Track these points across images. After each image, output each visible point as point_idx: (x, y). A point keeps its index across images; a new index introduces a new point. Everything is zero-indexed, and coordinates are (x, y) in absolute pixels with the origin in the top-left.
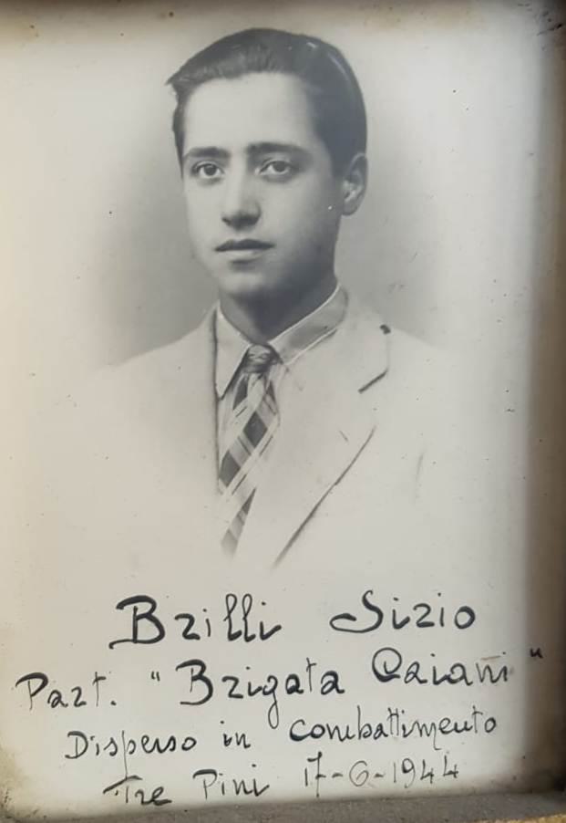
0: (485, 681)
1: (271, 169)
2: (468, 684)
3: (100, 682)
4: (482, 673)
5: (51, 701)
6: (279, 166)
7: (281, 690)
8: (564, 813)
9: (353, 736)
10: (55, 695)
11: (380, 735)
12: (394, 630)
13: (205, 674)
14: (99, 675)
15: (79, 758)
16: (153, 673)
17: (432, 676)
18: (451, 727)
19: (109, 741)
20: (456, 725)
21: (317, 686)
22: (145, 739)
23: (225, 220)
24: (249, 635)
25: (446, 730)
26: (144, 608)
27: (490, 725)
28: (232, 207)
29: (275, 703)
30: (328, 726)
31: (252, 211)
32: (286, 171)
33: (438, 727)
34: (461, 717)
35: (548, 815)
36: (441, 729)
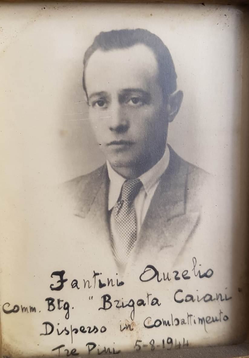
0: (218, 300)
1: (131, 103)
2: (159, 305)
6: (135, 101)
7: (136, 305)
8: (248, 354)
9: (114, 285)
10: (74, 282)
12: (17, 304)
13: (110, 301)
14: (189, 314)
15: (46, 336)
16: (90, 297)
17: (197, 298)
18: (211, 320)
20: (213, 318)
21: (150, 302)
22: (67, 317)
23: (111, 129)
24: (113, 285)
25: (208, 322)
27: (225, 318)
28: (115, 123)
29: (134, 310)
31: (124, 123)
32: (138, 104)
33: (205, 320)
35: (243, 356)
36: (207, 321)
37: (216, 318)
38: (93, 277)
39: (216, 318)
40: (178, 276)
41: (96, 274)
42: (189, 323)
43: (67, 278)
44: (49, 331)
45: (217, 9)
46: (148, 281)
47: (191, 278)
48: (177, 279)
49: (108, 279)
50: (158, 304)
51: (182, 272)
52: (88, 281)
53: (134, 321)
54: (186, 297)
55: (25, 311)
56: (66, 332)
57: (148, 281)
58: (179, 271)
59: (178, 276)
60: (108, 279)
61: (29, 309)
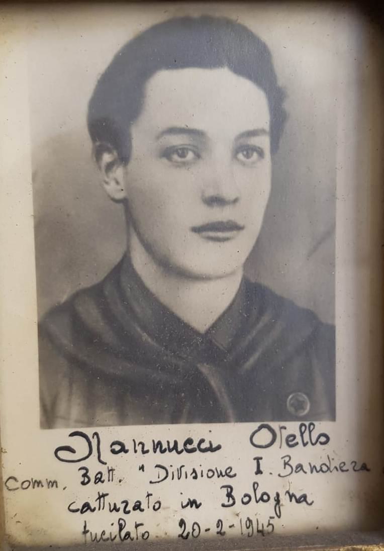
5: (243, 141)
11: (128, 538)
21: (151, 507)
26: (287, 459)
38: (96, 501)
42: (111, 479)
48: (195, 478)
51: (118, 521)
55: (155, 452)
61: (45, 483)
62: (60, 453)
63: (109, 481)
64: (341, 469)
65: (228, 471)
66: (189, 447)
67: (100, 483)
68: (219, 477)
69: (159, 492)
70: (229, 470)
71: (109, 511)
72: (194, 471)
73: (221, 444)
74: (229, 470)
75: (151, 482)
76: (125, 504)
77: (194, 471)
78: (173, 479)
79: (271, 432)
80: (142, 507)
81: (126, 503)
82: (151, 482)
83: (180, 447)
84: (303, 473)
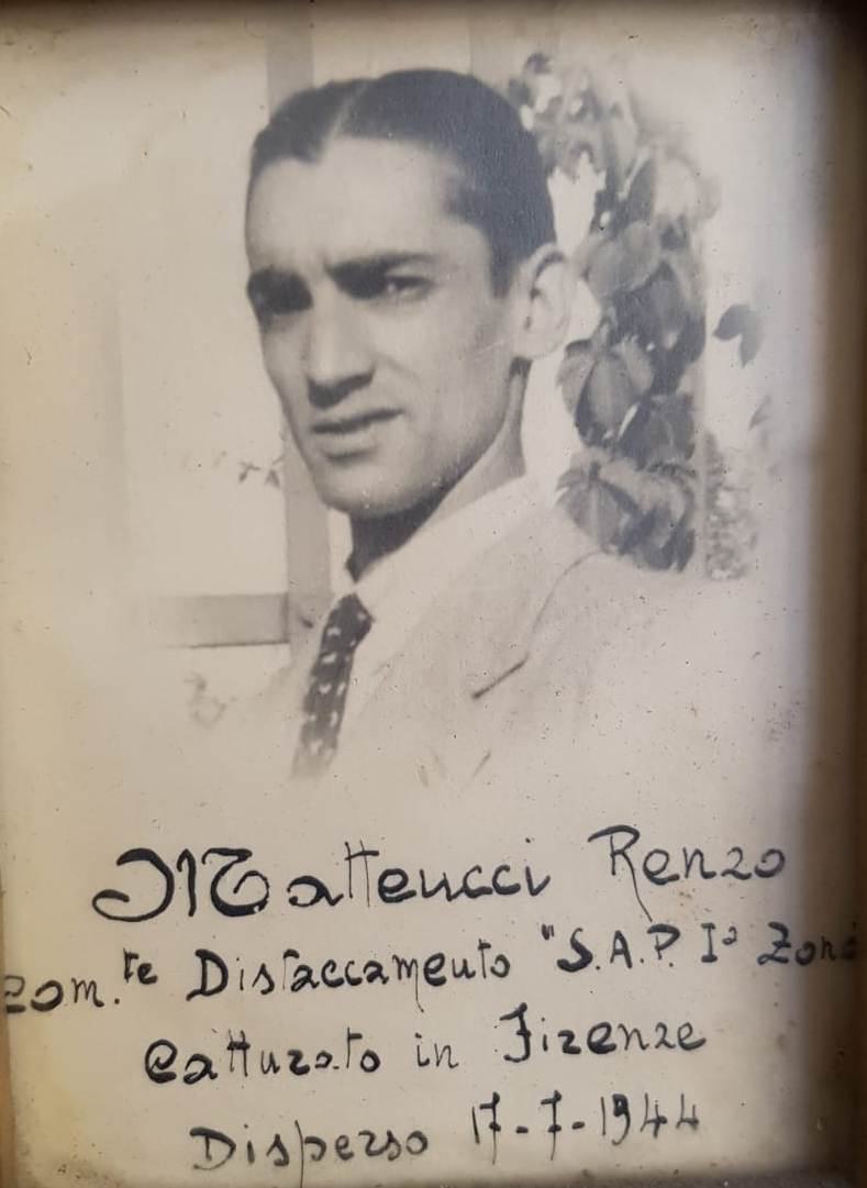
3: (485, 951)
4: (689, 858)
19: (258, 970)
27: (369, 1063)
30: (400, 977)
34: (460, 949)
37: (726, 536)
39: (726, 536)
40: (574, 1043)
41: (352, 1037)
43: (193, 955)
44: (212, 983)
45: (777, 984)
46: (109, 917)
47: (194, 951)
48: (570, 1049)
49: (685, 850)
50: (312, 982)
51: (586, 1036)
52: (636, 1031)
53: (30, 1013)
54: (409, 1138)
56: (263, 983)
57: (109, 917)
58: (575, 1032)
59: (574, 1043)
60: (685, 850)
62: (103, 904)
63: (232, 1069)
64: (590, 487)
65: (433, 965)
66: (331, 977)
67: (464, 977)
68: (414, 961)
69: (146, 941)
70: (438, 962)
71: (737, 929)
72: (277, 1143)
73: (700, 961)
74: (438, 962)
75: (508, 1058)
76: (367, 1138)
77: (277, 1143)
78: (191, 913)
79: (167, 894)
80: (385, 973)
81: (297, 1056)
82: (508, 1058)
83: (316, 977)
84: (626, 1026)
